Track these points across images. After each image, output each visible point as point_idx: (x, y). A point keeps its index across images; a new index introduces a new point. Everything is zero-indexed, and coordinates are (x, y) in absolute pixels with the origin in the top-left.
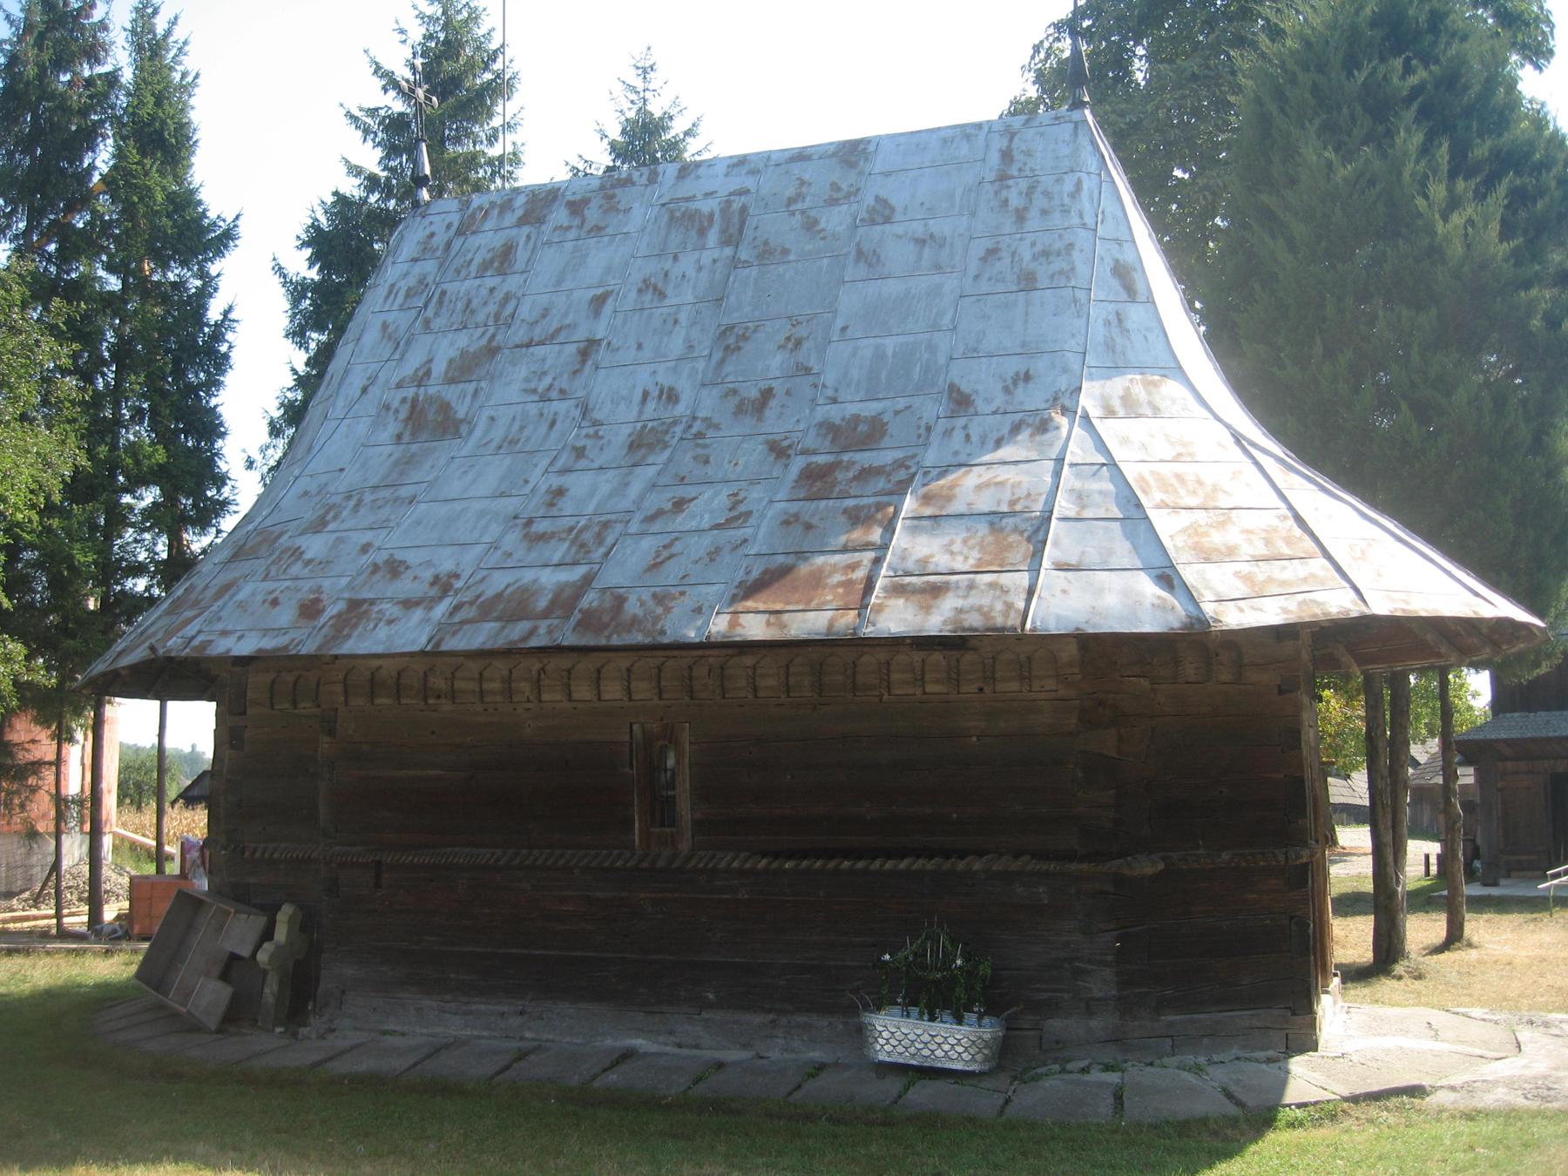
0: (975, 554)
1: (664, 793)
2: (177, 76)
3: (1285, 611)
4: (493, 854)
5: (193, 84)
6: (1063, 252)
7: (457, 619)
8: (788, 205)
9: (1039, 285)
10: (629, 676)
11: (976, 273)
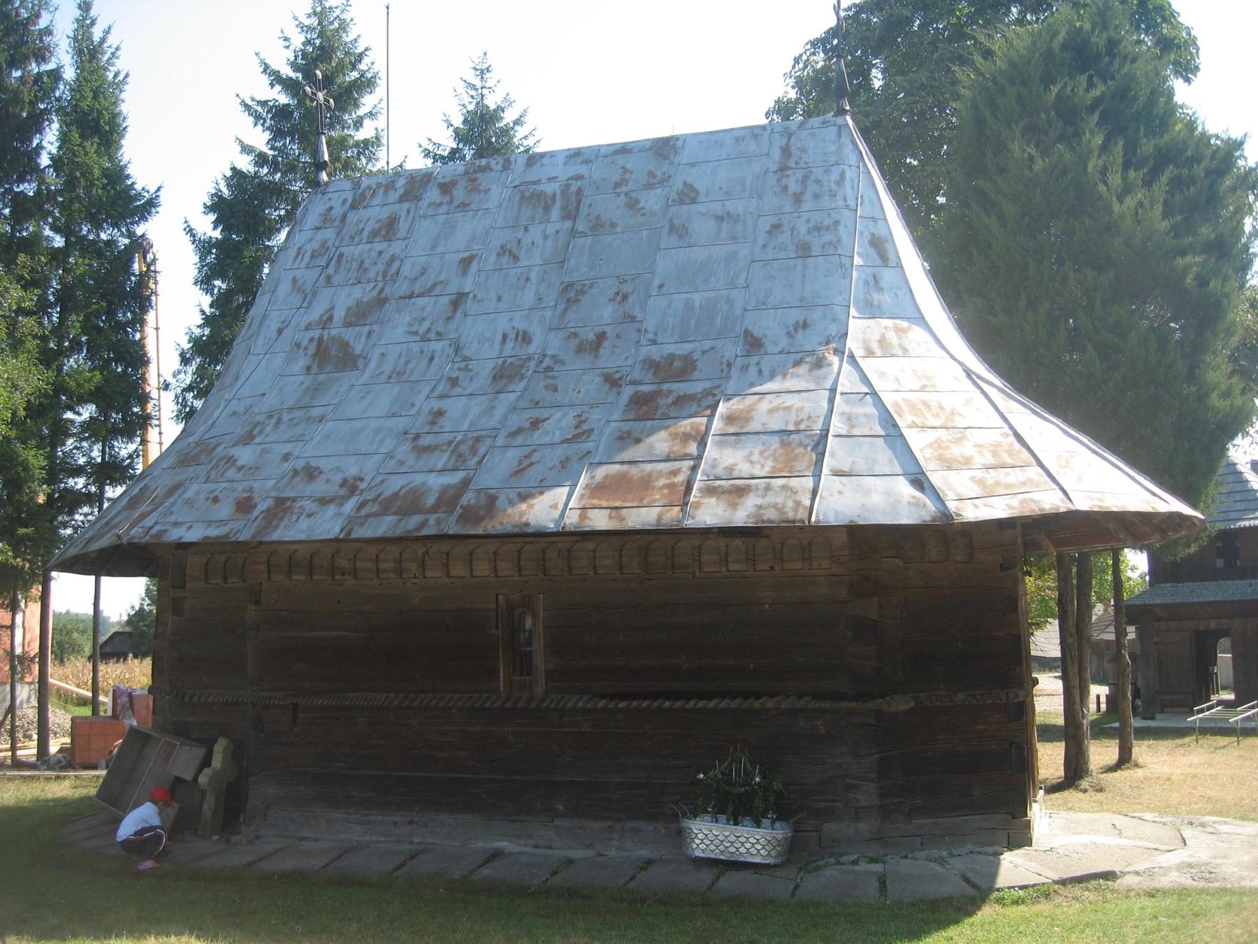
0: (770, 463)
1: (523, 649)
2: (110, 75)
3: (1010, 507)
4: (387, 698)
5: (124, 82)
6: (831, 227)
7: (363, 513)
8: (615, 188)
9: (813, 253)
10: (495, 558)
11: (764, 243)
